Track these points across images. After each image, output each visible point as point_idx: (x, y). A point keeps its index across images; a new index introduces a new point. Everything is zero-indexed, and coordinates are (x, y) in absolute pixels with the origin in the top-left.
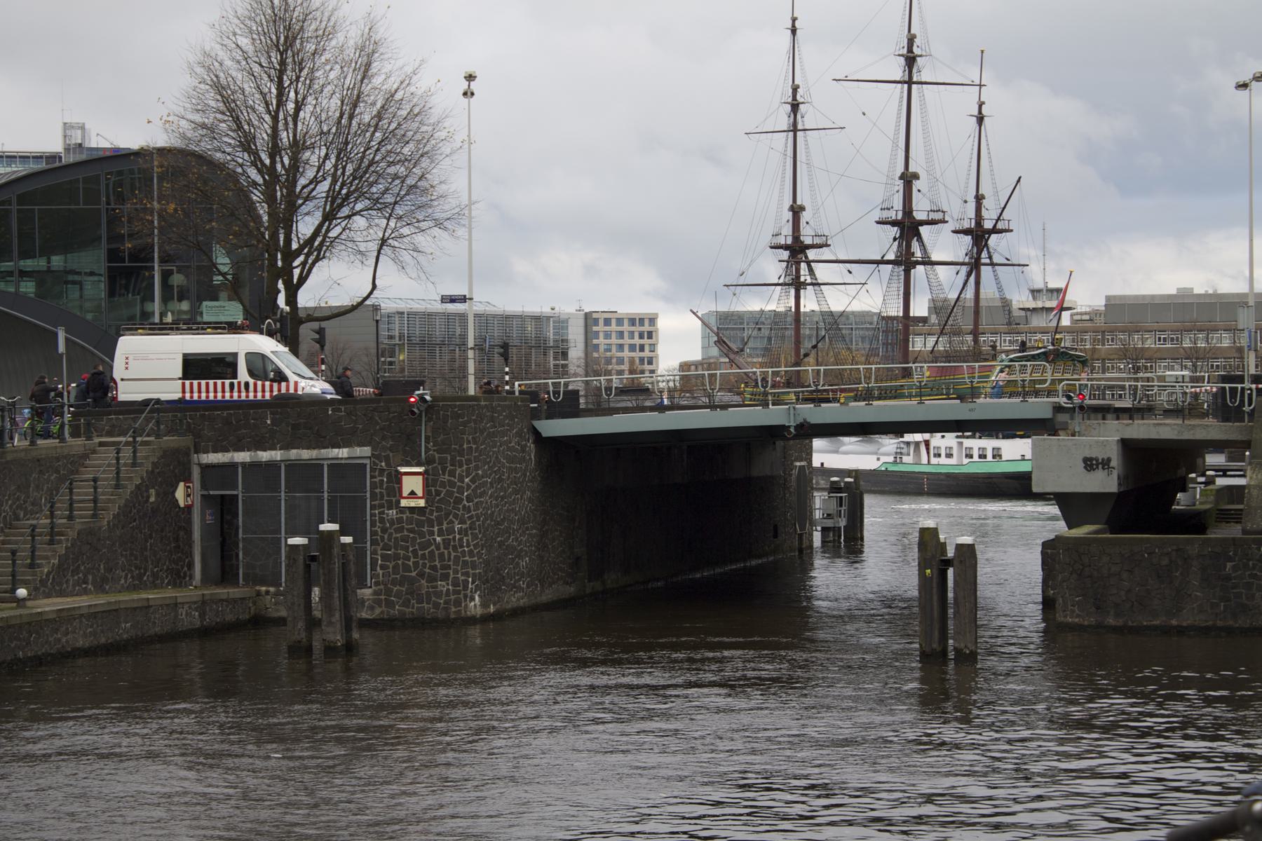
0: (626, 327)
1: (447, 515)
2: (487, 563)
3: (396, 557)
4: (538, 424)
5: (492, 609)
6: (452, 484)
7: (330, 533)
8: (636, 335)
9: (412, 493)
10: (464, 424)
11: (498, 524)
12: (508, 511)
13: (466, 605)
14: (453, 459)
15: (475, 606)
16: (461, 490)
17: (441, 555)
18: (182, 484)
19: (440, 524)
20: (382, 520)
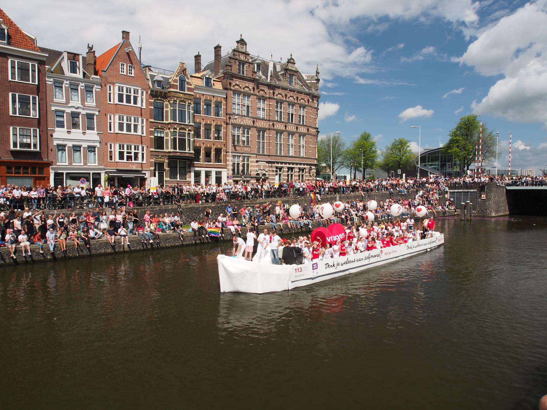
2: (496, 208)
3: (480, 206)
6: (490, 196)
7: (468, 203)
15: (493, 214)
16: (492, 197)
17: (488, 207)
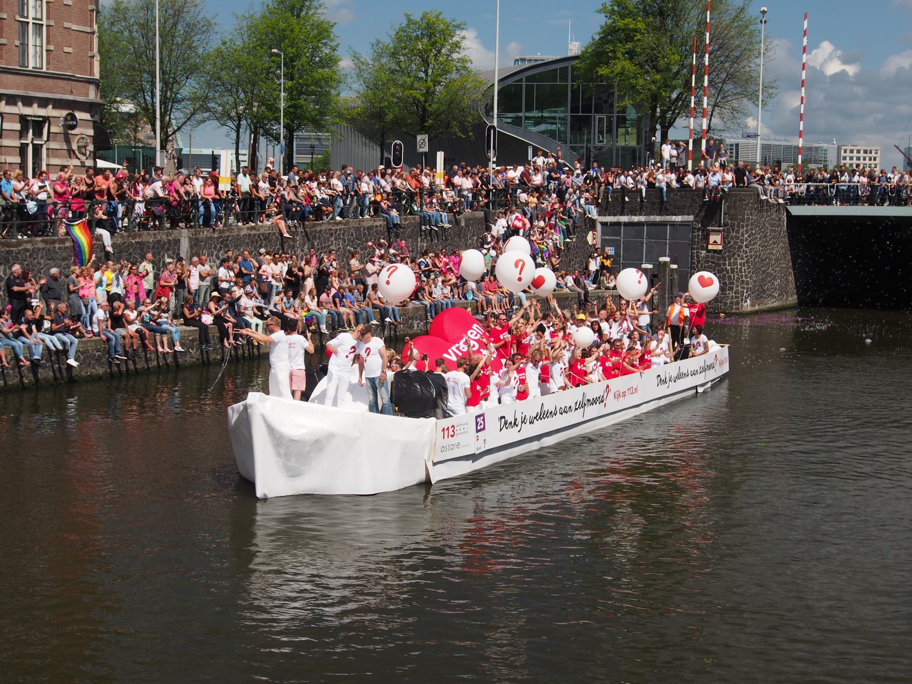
0: (862, 155)
1: (734, 255)
2: (755, 282)
4: (788, 207)
5: (757, 307)
6: (737, 238)
7: (665, 263)
8: (867, 159)
9: (715, 242)
10: (747, 205)
11: (763, 260)
12: (769, 253)
13: (742, 305)
14: (739, 224)
15: (747, 306)
16: (742, 242)
17: (730, 277)
18: (591, 233)
19: (730, 259)
20: (698, 257)
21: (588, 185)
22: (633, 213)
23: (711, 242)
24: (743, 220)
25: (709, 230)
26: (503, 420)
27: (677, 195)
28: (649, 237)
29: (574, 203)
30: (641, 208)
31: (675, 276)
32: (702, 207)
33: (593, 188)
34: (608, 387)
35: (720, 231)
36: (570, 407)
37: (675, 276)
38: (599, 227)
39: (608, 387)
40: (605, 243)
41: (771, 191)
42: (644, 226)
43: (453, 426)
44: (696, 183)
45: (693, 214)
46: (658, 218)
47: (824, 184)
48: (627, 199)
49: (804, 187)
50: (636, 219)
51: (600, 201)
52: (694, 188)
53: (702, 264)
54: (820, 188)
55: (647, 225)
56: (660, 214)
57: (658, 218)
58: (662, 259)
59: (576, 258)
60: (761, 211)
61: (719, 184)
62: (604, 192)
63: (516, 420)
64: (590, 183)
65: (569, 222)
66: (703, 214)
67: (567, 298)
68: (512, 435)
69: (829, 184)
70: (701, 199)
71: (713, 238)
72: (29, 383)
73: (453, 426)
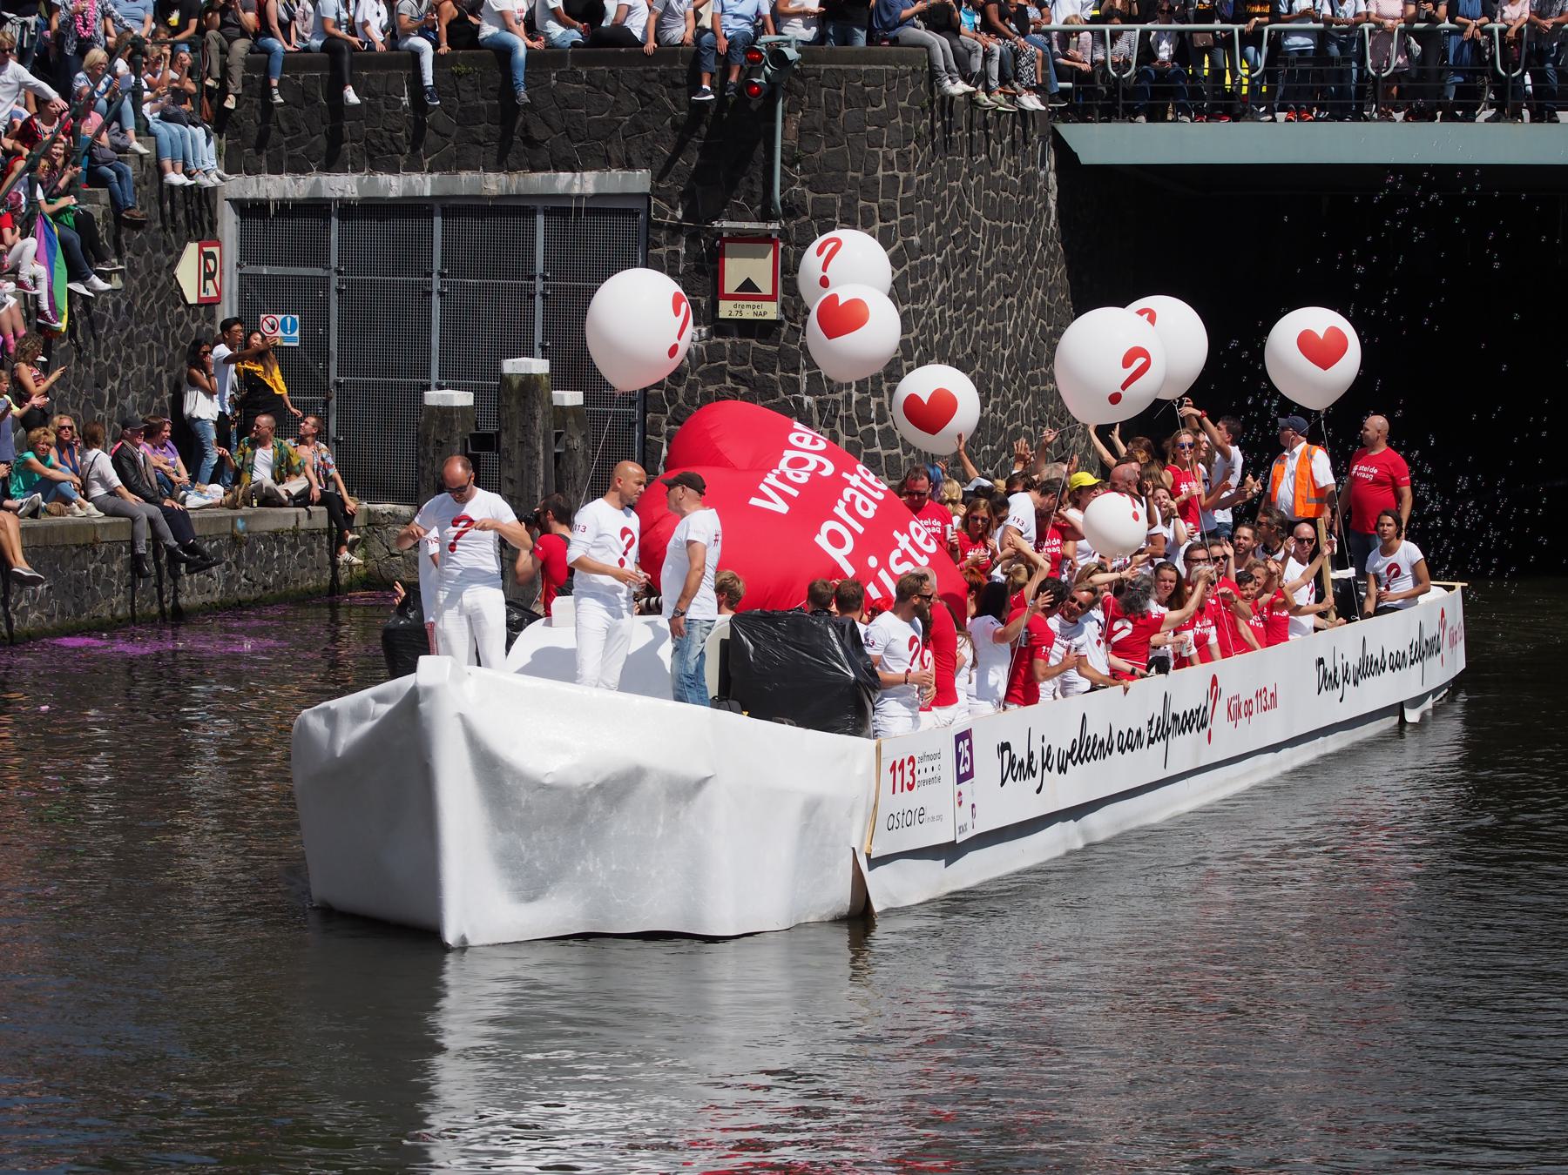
7: (530, 381)
9: (748, 286)
10: (882, 121)
12: (985, 335)
18: (192, 249)
21: (176, 31)
22: (379, 159)
23: (731, 284)
24: (868, 190)
25: (718, 234)
26: (1006, 753)
27: (576, 77)
28: (453, 267)
29: (114, 116)
30: (417, 140)
31: (577, 442)
32: (684, 131)
33: (197, 45)
34: (1214, 681)
35: (766, 238)
36: (1139, 733)
37: (577, 442)
38: (229, 223)
39: (1214, 681)
40: (257, 295)
41: (988, 56)
42: (532, 213)
43: (912, 759)
44: (660, 25)
45: (648, 162)
46: (494, 183)
47: (1217, 25)
48: (351, 96)
49: (1128, 45)
50: (394, 185)
51: (230, 103)
52: (651, 46)
53: (692, 387)
54: (1200, 41)
55: (548, 213)
56: (501, 165)
57: (494, 183)
58: (511, 366)
59: (128, 364)
60: (948, 145)
61: (760, 30)
62: (249, 65)
63: (1031, 756)
64: (183, 24)
65: (92, 199)
66: (690, 161)
67: (91, 547)
68: (1021, 802)
69: (1236, 28)
70: (683, 91)
71: (736, 270)
72: (1175, 444)
73: (912, 759)
